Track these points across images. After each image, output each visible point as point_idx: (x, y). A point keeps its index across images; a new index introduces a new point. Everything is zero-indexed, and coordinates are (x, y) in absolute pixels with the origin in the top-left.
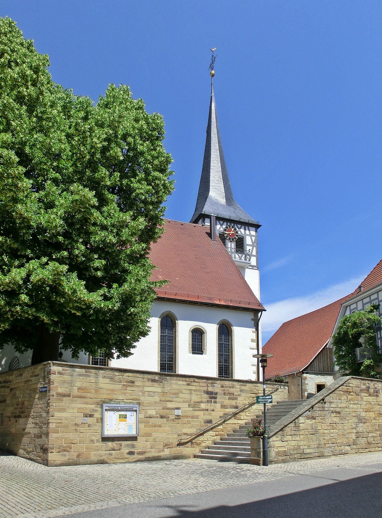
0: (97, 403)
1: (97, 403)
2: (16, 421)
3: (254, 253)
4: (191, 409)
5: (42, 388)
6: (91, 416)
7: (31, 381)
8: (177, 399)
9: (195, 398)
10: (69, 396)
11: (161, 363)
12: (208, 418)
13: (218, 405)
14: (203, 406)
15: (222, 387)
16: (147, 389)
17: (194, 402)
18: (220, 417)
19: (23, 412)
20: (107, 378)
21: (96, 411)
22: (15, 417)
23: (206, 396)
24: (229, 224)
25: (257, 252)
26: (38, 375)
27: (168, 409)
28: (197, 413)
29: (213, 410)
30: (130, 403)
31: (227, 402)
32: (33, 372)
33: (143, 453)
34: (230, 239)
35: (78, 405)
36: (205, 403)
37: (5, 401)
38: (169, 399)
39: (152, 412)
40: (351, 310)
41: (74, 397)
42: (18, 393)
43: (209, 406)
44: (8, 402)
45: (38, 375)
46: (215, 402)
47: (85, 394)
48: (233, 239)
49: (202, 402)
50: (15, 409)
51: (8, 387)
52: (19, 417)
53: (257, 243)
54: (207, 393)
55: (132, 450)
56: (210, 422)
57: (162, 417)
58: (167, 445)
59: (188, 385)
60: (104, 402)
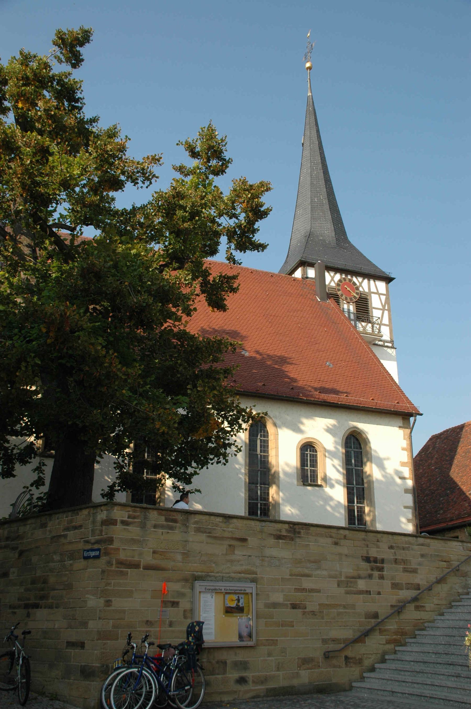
0: (186, 580)
1: (186, 580)
2: (28, 615)
3: (386, 320)
4: (342, 590)
5: (88, 551)
6: (175, 604)
7: (65, 536)
8: (318, 572)
9: (347, 569)
10: (136, 566)
11: (249, 503)
12: (372, 608)
13: (387, 583)
14: (362, 584)
15: (391, 547)
16: (269, 552)
17: (347, 577)
18: (392, 606)
19: (42, 598)
20: (203, 532)
21: (183, 595)
22: (27, 606)
23: (364, 565)
24: (344, 276)
25: (390, 319)
26: (80, 527)
27: (304, 590)
28: (351, 599)
29: (379, 593)
30: (239, 580)
31: (403, 578)
32: (71, 521)
33: (264, 681)
34: (346, 299)
35: (153, 582)
36: (365, 578)
37: (5, 575)
38: (306, 571)
39: (278, 597)
40: (149, 355)
41: (147, 568)
42: (35, 559)
43: (374, 585)
44: (12, 577)
45: (80, 527)
46: (382, 577)
47: (163, 563)
48: (351, 299)
49: (359, 577)
50: (27, 590)
51: (14, 549)
52: (36, 606)
53: (388, 305)
54: (367, 559)
55: (244, 674)
56: (376, 616)
57: (294, 606)
58: (306, 662)
59: (336, 544)
60: (196, 578)
